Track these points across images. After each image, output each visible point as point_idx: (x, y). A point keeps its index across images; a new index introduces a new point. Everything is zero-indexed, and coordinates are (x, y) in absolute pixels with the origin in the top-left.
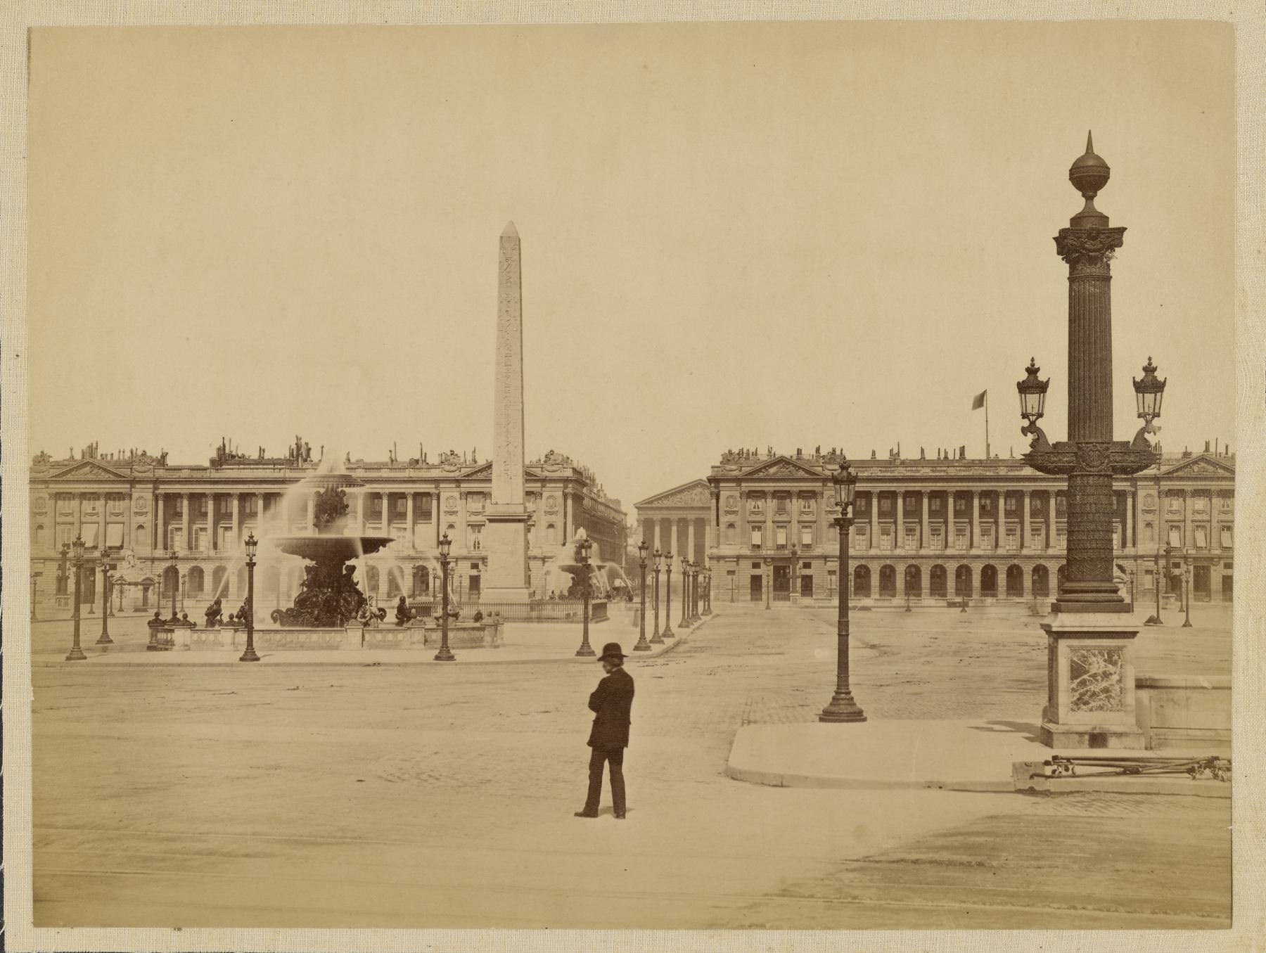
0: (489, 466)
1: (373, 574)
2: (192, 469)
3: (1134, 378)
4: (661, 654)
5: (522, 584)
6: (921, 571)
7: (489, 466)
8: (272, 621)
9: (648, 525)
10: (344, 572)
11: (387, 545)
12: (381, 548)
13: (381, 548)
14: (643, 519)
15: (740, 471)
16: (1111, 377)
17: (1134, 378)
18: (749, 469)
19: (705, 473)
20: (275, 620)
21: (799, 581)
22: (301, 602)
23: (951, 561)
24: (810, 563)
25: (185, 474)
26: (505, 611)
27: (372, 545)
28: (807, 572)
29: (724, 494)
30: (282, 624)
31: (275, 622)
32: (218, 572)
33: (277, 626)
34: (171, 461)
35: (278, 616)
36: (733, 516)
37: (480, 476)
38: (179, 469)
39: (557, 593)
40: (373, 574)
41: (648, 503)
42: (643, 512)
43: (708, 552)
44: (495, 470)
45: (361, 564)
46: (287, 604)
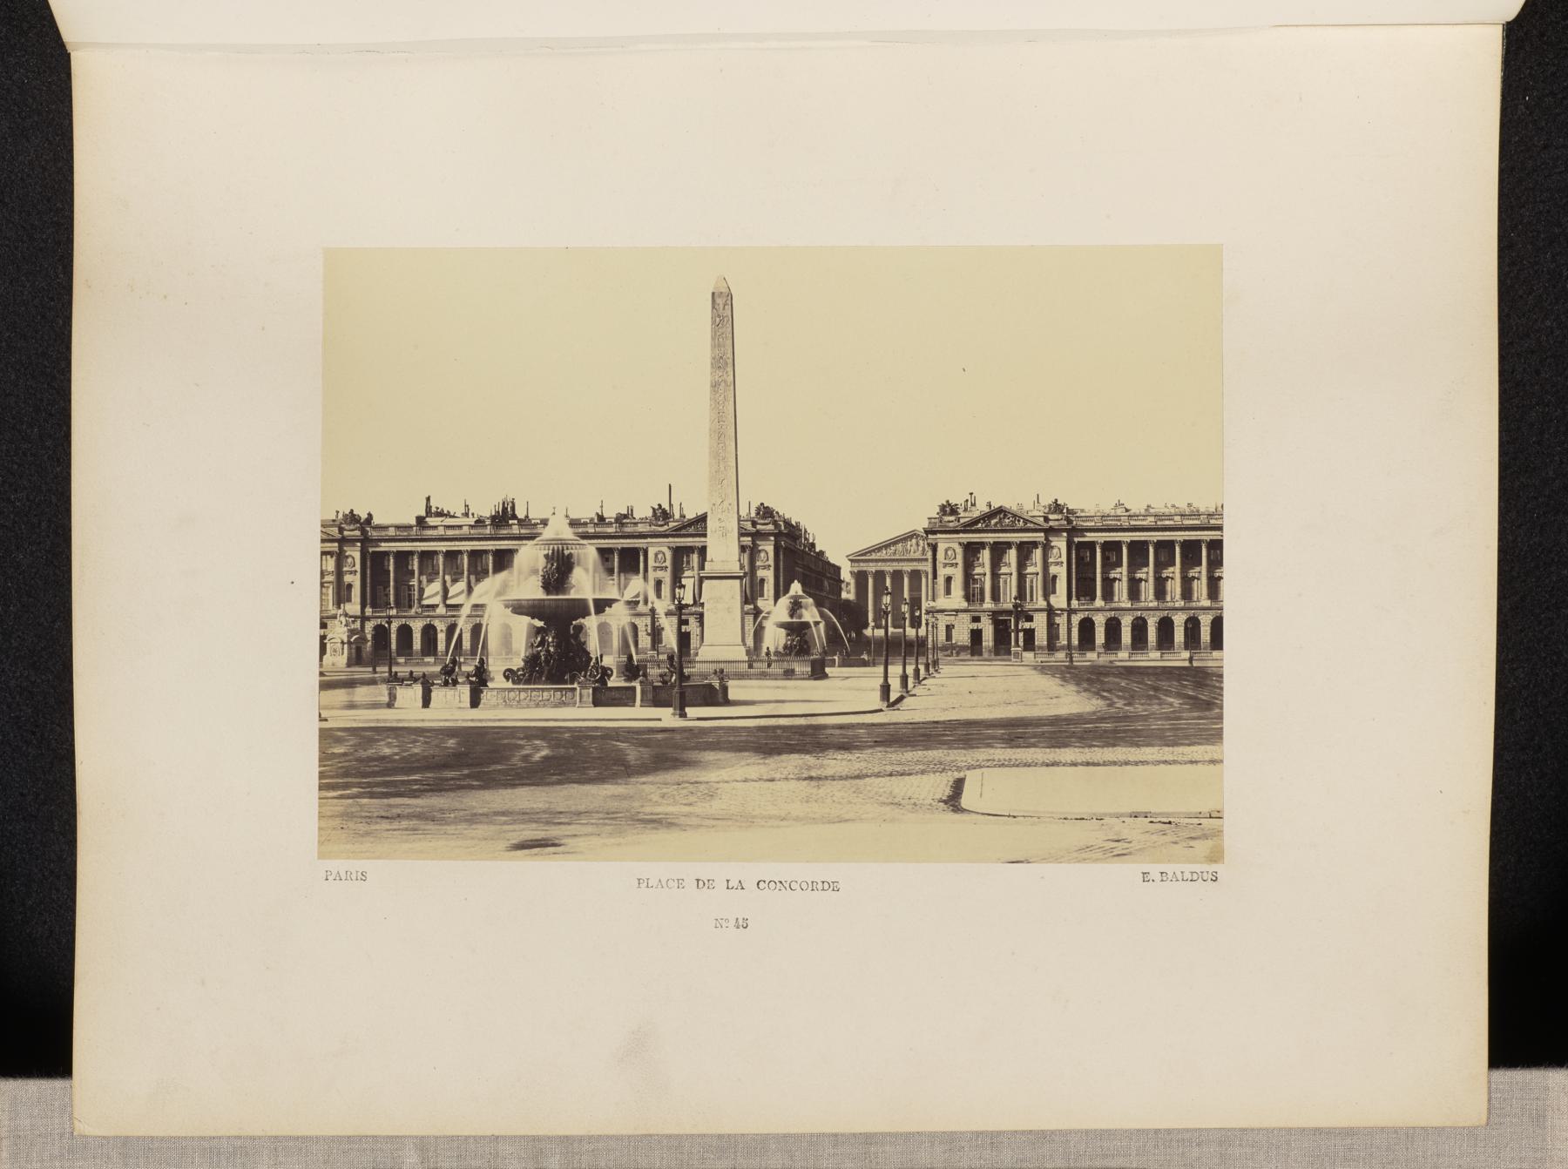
0: (702, 519)
1: (603, 629)
2: (398, 527)
3: (428, 499)
4: (1007, 726)
5: (739, 640)
6: (1120, 624)
7: (702, 519)
8: (505, 680)
9: (860, 577)
10: (572, 632)
11: (613, 605)
12: (607, 609)
13: (607, 609)
14: (856, 571)
15: (959, 521)
16: (70, 530)
17: (428, 499)
18: (676, 524)
19: (921, 525)
20: (507, 678)
21: (1021, 634)
22: (532, 662)
23: (1180, 613)
24: (980, 617)
25: (392, 532)
26: (728, 669)
27: (602, 605)
28: (1027, 625)
29: (941, 548)
30: (514, 683)
31: (508, 680)
32: (451, 629)
33: (510, 685)
34: (376, 521)
35: (509, 674)
36: (952, 568)
37: (691, 530)
38: (386, 528)
39: (772, 650)
40: (603, 629)
41: (862, 555)
42: (856, 564)
43: (925, 605)
44: (711, 524)
45: (591, 623)
46: (517, 663)
